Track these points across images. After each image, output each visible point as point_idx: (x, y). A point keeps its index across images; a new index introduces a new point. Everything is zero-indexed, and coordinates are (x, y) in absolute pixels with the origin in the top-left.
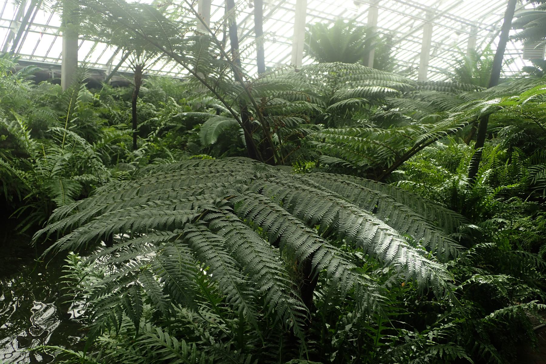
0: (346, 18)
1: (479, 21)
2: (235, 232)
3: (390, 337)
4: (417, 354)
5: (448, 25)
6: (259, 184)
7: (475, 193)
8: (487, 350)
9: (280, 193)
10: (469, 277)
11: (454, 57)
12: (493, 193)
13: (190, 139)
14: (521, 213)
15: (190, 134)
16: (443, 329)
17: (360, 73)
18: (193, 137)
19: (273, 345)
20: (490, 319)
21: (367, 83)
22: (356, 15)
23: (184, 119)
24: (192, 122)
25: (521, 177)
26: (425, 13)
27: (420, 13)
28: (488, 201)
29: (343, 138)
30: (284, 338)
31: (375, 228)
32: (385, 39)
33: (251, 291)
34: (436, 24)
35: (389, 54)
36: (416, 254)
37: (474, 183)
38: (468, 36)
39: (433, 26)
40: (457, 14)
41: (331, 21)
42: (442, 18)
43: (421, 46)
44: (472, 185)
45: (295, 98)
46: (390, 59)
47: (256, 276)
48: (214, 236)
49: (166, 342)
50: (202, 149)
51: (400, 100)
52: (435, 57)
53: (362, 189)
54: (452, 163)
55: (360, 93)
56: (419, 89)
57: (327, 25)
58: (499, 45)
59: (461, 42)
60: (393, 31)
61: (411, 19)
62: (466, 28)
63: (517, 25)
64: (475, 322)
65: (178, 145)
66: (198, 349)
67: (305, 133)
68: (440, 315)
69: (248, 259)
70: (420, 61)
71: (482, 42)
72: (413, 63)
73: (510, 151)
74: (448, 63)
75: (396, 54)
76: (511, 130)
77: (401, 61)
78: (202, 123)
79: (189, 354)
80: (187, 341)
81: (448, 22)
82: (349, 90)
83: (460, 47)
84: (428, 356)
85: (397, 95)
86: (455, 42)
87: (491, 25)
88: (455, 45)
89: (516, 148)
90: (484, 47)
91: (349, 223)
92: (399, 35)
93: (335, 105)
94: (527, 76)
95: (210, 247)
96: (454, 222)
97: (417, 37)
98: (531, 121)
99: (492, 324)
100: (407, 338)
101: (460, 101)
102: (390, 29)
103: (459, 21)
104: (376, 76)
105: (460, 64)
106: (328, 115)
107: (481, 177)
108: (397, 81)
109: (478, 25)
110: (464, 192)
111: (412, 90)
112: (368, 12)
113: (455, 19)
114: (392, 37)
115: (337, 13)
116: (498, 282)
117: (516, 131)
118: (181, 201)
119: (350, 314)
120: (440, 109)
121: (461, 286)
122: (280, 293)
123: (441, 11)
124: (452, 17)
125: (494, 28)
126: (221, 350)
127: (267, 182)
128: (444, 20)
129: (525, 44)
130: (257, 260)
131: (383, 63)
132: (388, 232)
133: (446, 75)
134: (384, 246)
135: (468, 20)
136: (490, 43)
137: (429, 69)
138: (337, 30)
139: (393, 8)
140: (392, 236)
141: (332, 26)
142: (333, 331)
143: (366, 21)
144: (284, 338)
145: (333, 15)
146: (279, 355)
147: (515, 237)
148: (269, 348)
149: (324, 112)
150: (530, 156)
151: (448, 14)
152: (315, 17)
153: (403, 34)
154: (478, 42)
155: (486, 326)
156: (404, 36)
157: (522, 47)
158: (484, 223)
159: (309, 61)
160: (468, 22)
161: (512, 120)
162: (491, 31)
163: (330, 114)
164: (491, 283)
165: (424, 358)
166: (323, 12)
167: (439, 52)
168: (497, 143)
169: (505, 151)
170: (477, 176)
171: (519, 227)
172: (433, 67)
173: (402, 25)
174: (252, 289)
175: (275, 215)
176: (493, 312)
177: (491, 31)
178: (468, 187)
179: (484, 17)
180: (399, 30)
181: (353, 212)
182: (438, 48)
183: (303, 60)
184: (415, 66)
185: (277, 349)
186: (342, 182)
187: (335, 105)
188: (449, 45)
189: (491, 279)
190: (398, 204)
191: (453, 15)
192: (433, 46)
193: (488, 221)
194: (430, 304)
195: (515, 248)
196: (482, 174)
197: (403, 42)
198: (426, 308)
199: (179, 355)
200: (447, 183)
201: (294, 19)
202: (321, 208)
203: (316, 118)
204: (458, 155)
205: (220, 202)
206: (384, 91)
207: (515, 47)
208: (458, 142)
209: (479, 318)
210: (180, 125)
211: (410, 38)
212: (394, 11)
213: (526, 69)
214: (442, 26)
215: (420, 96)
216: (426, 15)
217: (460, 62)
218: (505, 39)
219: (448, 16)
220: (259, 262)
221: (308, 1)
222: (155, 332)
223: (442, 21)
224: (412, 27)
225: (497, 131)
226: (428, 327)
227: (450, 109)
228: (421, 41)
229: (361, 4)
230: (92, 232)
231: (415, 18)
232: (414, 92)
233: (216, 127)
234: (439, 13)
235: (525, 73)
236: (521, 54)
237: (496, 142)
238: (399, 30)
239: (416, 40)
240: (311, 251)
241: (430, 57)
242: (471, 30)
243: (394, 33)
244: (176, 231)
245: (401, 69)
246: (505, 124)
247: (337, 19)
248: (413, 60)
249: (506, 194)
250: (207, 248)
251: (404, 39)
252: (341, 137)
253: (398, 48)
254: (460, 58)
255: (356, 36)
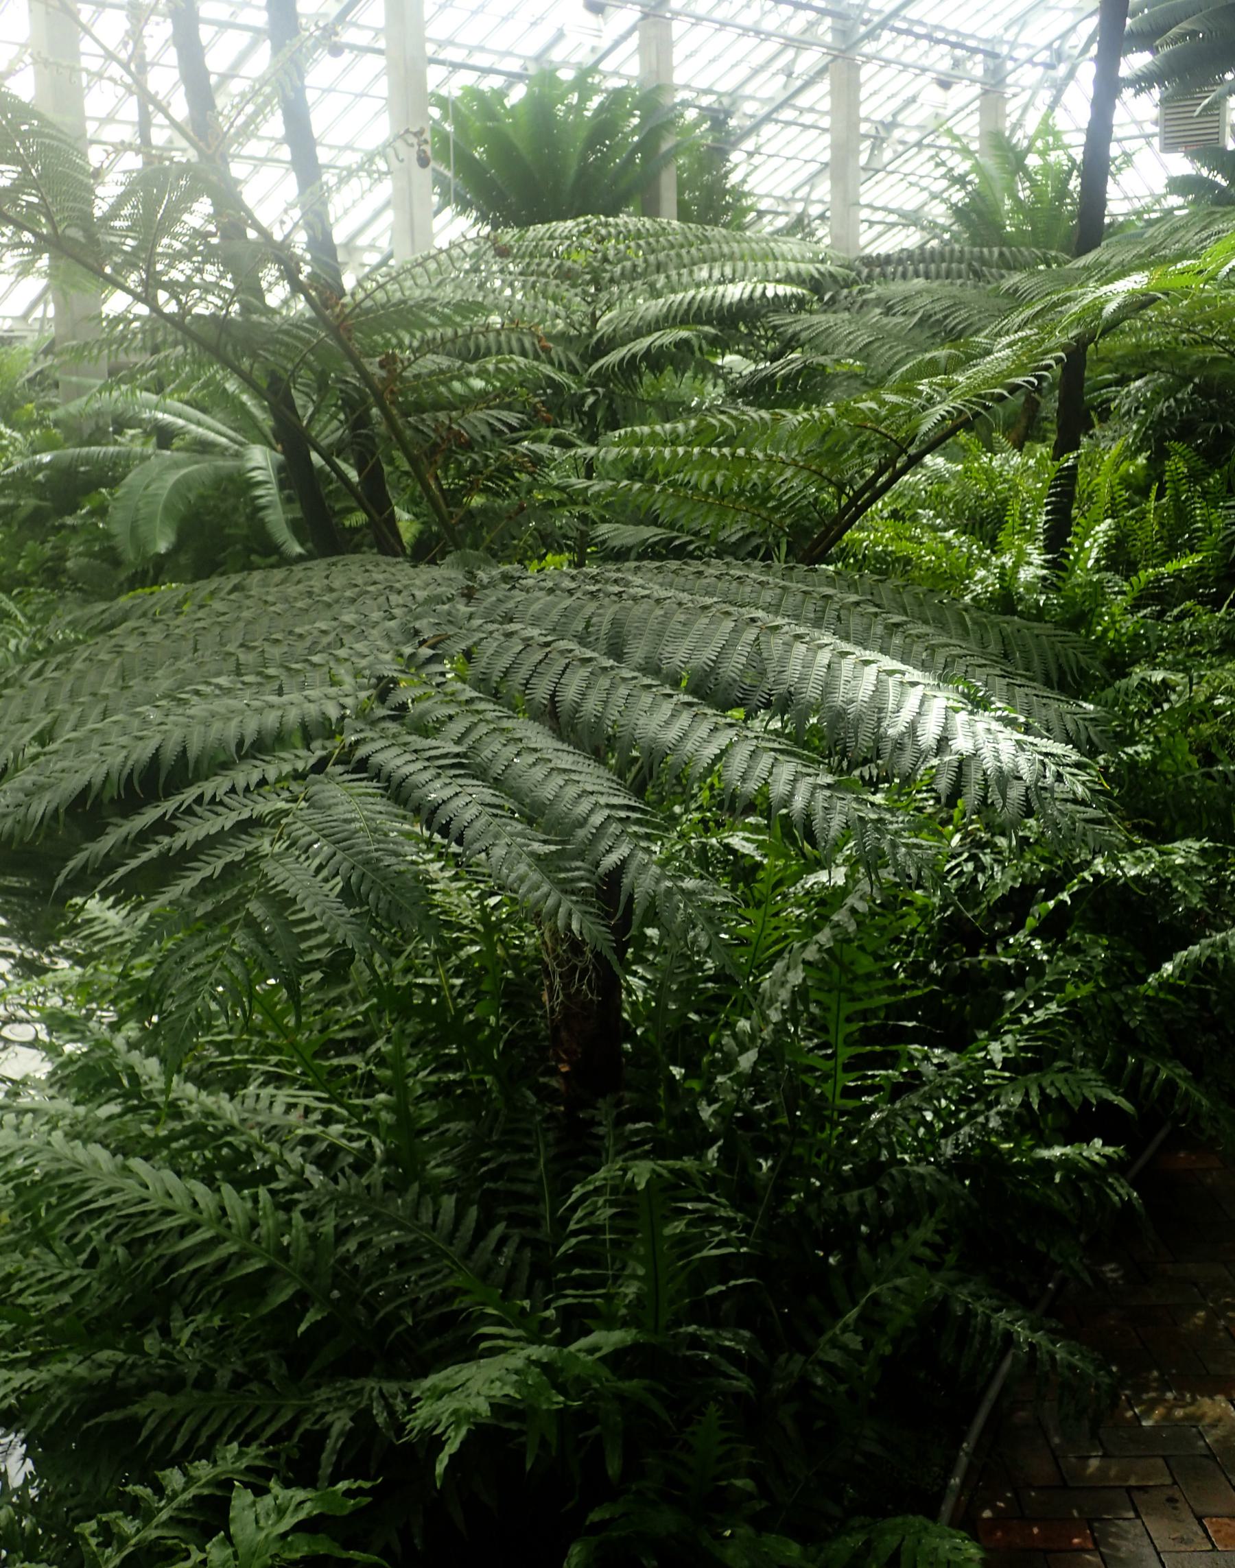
0: (565, 64)
1: (1009, 36)
2: (483, 729)
3: (874, 1076)
4: (962, 1116)
5: (908, 58)
6: (499, 600)
7: (1070, 602)
8: (1163, 1075)
9: (567, 614)
10: (1087, 864)
11: (943, 163)
12: (1124, 593)
13: (75, 547)
14: (1214, 653)
15: (74, 529)
16: (1031, 1025)
17: (672, 246)
18: (82, 537)
19: (517, 1157)
20: (1163, 985)
21: (704, 274)
22: (601, 53)
23: (40, 477)
24: (71, 488)
25: (1200, 539)
26: (828, 21)
27: (811, 25)
28: (1114, 622)
29: (675, 454)
30: (548, 1129)
31: (870, 673)
32: (705, 126)
33: (578, 869)
34: (869, 58)
35: (726, 176)
36: (996, 726)
37: (1063, 568)
38: (977, 89)
39: (859, 68)
40: (931, 20)
41: (514, 78)
42: (886, 35)
43: (827, 139)
44: (1058, 576)
45: (478, 347)
46: (726, 192)
47: (581, 833)
48: (434, 743)
49: (170, 1196)
50: (123, 575)
51: (816, 319)
52: (877, 171)
53: (784, 588)
54: (982, 519)
55: (687, 311)
56: (869, 278)
57: (501, 94)
58: (1114, 107)
59: (957, 112)
60: (730, 94)
61: (786, 46)
62: (969, 65)
63: (1145, 39)
64: (1119, 998)
65: (35, 573)
66: (278, 1206)
67: (537, 461)
68: (1011, 995)
69: (548, 792)
70: (832, 191)
71: (1025, 109)
72: (807, 200)
73: (1159, 457)
74: (923, 189)
75: (748, 175)
76: (1154, 392)
77: (767, 196)
78: (114, 483)
79: (254, 1225)
80: (238, 1185)
81: (906, 48)
82: (650, 307)
83: (957, 131)
84: (998, 1113)
85: (801, 302)
86: (937, 115)
87: (1049, 47)
88: (939, 126)
89: (1176, 445)
90: (1032, 124)
91: (794, 670)
92: (749, 107)
93: (613, 357)
94: (1180, 208)
95: (433, 772)
96: (1057, 656)
97: (811, 110)
98: (1213, 351)
99: (1171, 998)
100: (928, 1069)
101: (1004, 303)
102: (715, 88)
103: (944, 41)
104: (726, 249)
105: (963, 187)
106: (595, 393)
107: (1082, 549)
108: (794, 260)
109: (1004, 50)
110: (1037, 601)
111: (848, 284)
112: (636, 34)
113: (929, 37)
114: (729, 114)
115: (532, 47)
116: (1173, 868)
117: (1167, 392)
118: (289, 669)
119: (744, 1025)
120: (951, 333)
121: (1065, 896)
122: (655, 869)
123: (880, 12)
124: (918, 29)
125: (1059, 56)
126: (355, 1197)
127: (516, 592)
128: (893, 42)
129: (1164, 102)
130: (572, 791)
131: (713, 204)
132: (907, 678)
133: (923, 228)
134: (906, 715)
135: (972, 36)
136: (1052, 108)
137: (865, 214)
138: (541, 108)
139: (719, 14)
140: (920, 687)
141: (517, 94)
142: (696, 1085)
143: (633, 68)
144: (548, 1129)
145: (520, 57)
146: (540, 1178)
147: (1206, 729)
148: (503, 1167)
149: (580, 383)
150: (1221, 467)
151: (905, 19)
152: (456, 66)
153: (764, 101)
154: (1013, 108)
155: (1153, 1006)
156: (767, 109)
157: (1155, 113)
158: (1109, 693)
159: (456, 228)
160: (971, 43)
161: (1154, 354)
162: (1050, 66)
163: (600, 390)
164: (1154, 874)
165: (987, 1119)
166: (481, 49)
167: (887, 155)
168: (1113, 439)
169: (1141, 460)
170: (1070, 545)
171: (1211, 698)
172: (876, 209)
173: (756, 72)
174: (579, 864)
175: (584, 672)
176: (1170, 959)
177: (1050, 66)
178: (1046, 585)
179: (1021, 21)
180: (748, 90)
181: (798, 637)
182: (883, 140)
183: (438, 223)
184: (815, 210)
185: (532, 1164)
186: (719, 578)
187: (613, 357)
188: (919, 127)
189: (1150, 859)
190: (897, 619)
191: (920, 23)
192: (866, 136)
193: (1121, 684)
194: (976, 967)
195: (1209, 759)
196: (1086, 539)
197: (768, 130)
198: (962, 982)
199: (223, 1231)
200: (982, 581)
201: (384, 80)
202: (704, 639)
203: (554, 407)
204: (998, 493)
205: (413, 655)
206: (764, 293)
207: (1139, 111)
208: (991, 448)
209: (1129, 982)
210: (29, 503)
211: (787, 114)
212: (723, 25)
213: (1179, 185)
214: (888, 62)
215: (879, 301)
216: (833, 29)
217: (961, 181)
218: (1108, 89)
219: (904, 26)
220: (580, 796)
221: (428, 10)
222: (126, 1171)
223: (888, 45)
224: (789, 75)
225: (1109, 400)
226: (982, 1035)
227: (985, 327)
228: (826, 122)
229: (609, 10)
230: (63, 785)
231: (798, 44)
232: (855, 289)
233: (165, 493)
234: (876, 19)
235: (1175, 200)
236: (1153, 135)
237: (1110, 433)
238: (748, 90)
239: (808, 119)
240: (712, 750)
241: (863, 176)
242: (985, 71)
243: (733, 103)
244: (316, 744)
245: (771, 223)
246: (1133, 372)
247: (532, 70)
248: (806, 189)
249: (1158, 597)
250: (427, 775)
251: (767, 118)
252: (667, 452)
253: (750, 155)
254: (962, 166)
255: (605, 127)
